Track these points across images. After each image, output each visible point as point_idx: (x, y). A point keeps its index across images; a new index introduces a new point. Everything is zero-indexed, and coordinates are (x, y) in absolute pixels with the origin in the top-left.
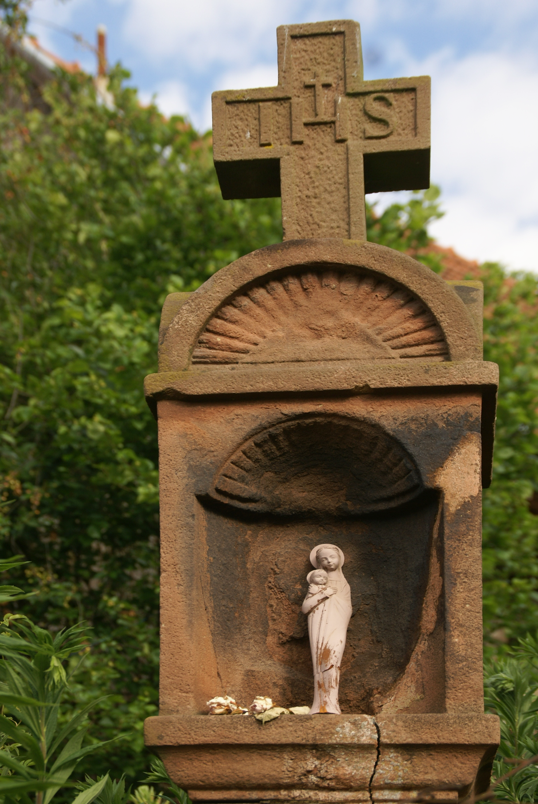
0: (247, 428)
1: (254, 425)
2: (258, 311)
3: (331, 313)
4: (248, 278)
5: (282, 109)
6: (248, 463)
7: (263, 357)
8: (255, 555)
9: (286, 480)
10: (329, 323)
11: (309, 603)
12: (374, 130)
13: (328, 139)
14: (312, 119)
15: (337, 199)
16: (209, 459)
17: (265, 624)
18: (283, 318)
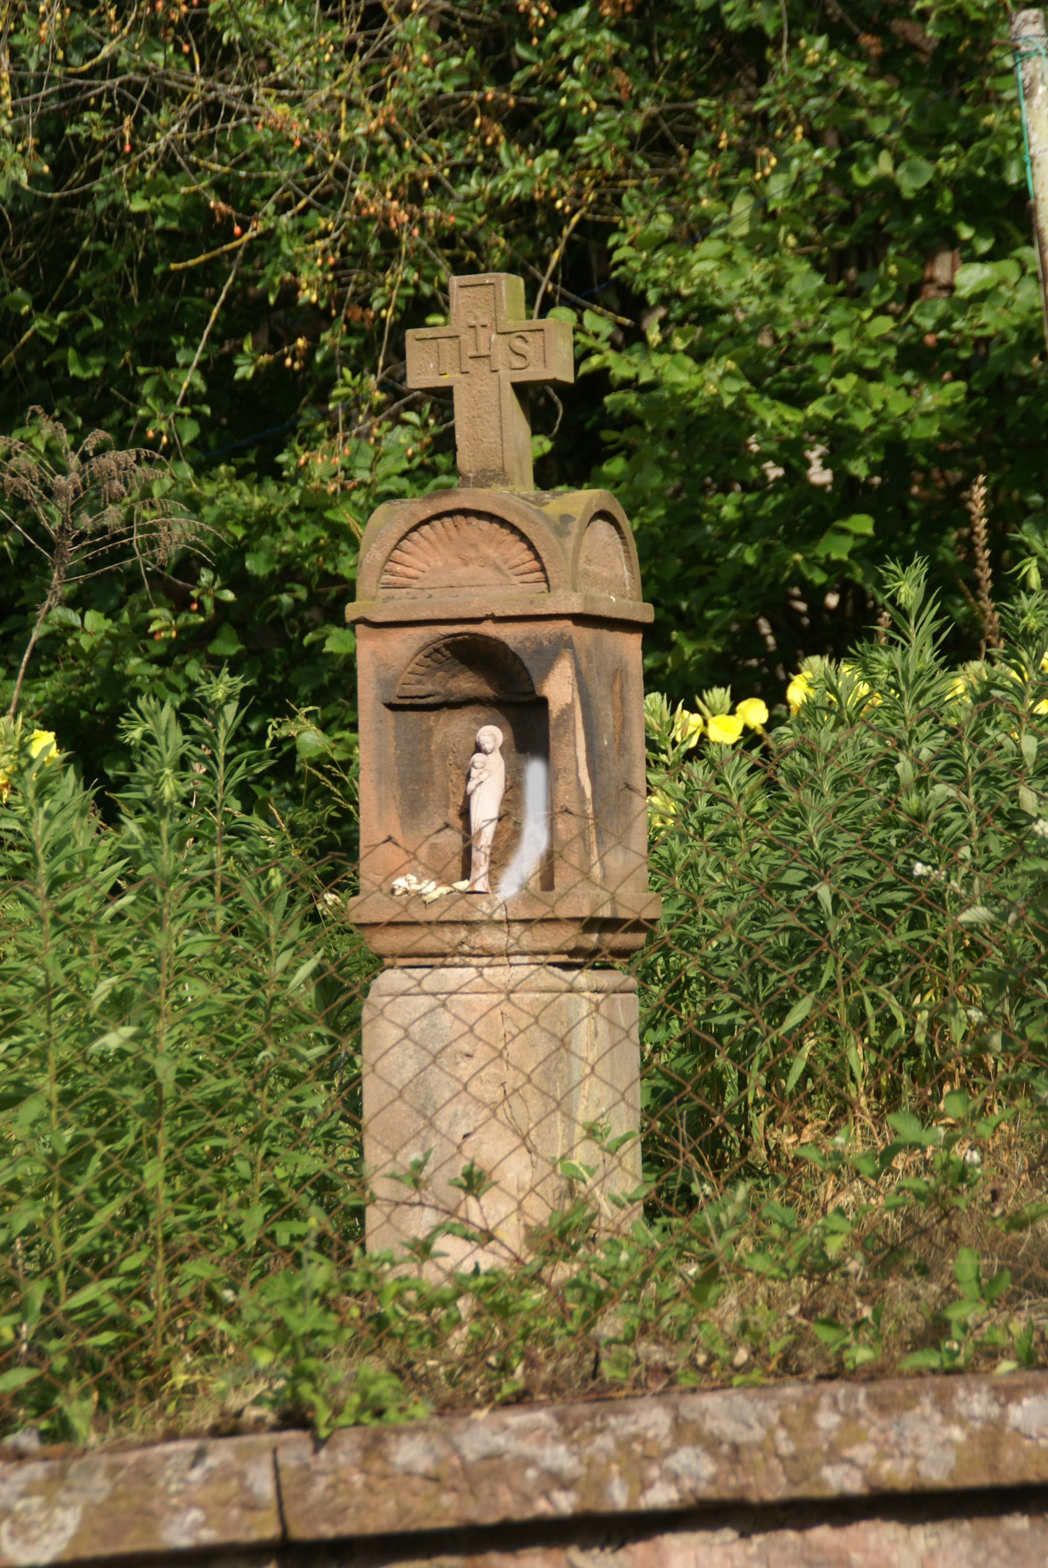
0: (417, 646)
1: (421, 644)
2: (425, 544)
3: (474, 546)
4: (416, 521)
5: (453, 343)
6: (422, 670)
7: (426, 584)
8: (438, 738)
9: (454, 676)
10: (472, 554)
11: (471, 785)
12: (517, 362)
13: (487, 368)
14: (474, 353)
15: (494, 419)
16: (391, 672)
17: (447, 798)
18: (442, 549)
